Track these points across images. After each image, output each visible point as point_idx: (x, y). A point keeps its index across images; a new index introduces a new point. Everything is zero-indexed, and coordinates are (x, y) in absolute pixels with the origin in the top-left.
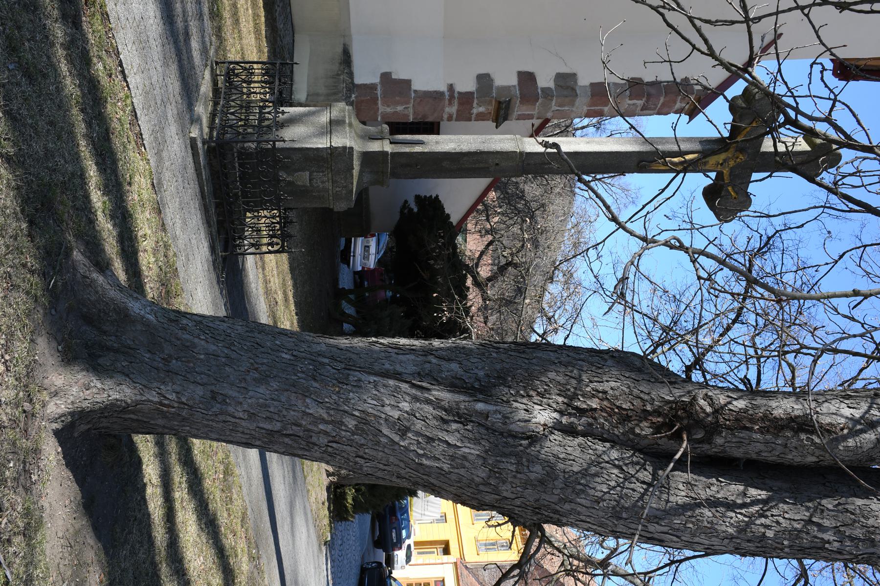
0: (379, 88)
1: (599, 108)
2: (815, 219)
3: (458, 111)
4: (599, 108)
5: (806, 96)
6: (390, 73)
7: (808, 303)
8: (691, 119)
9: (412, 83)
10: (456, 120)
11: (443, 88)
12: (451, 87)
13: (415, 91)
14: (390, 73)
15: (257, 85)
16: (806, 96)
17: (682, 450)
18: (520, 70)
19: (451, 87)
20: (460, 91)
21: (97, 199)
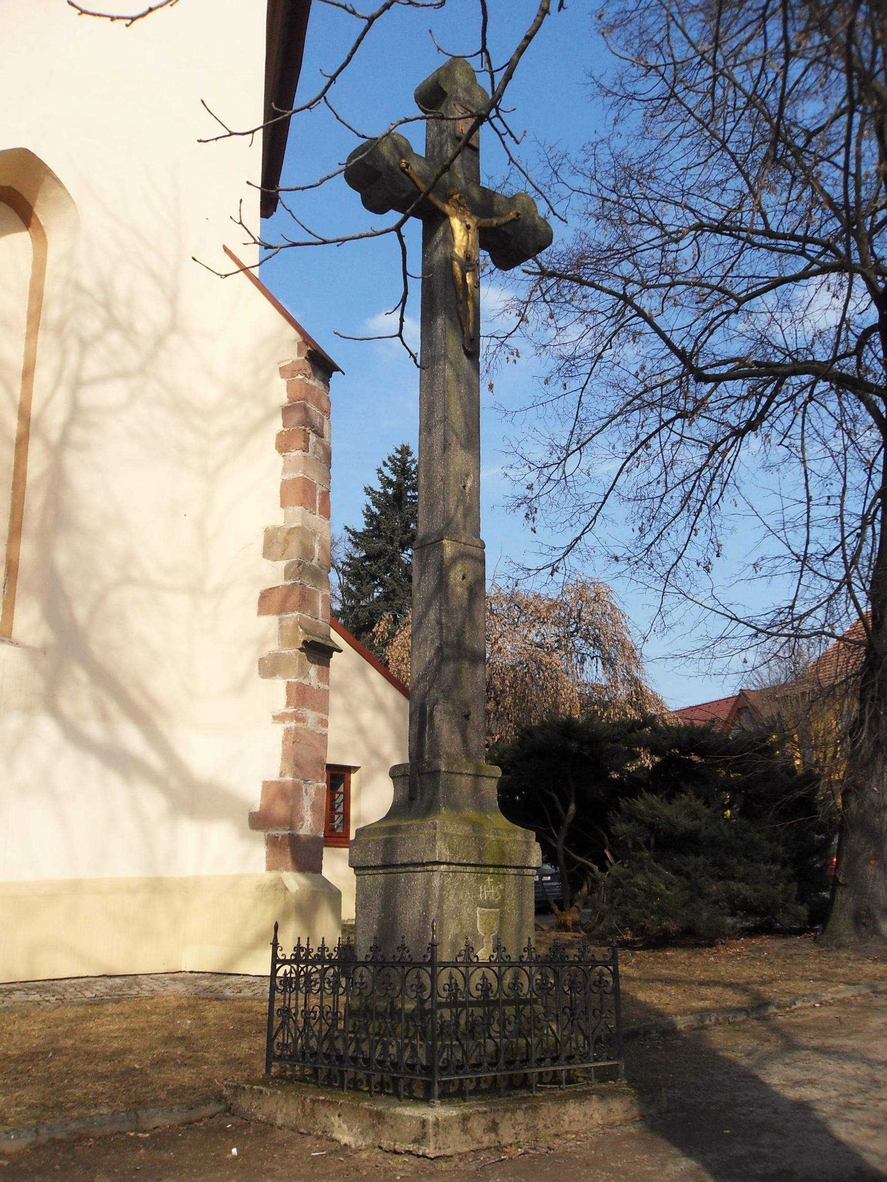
0: (275, 833)
1: (318, 497)
2: (231, 134)
3: (314, 709)
4: (318, 497)
5: (400, 237)
6: (251, 814)
7: (714, 281)
8: (338, 369)
9: (268, 779)
10: (327, 714)
11: (279, 730)
12: (279, 718)
13: (282, 774)
14: (251, 814)
15: (301, 1002)
16: (400, 237)
17: (318, 506)
18: (256, 612)
19: (279, 718)
20: (285, 703)
21: (878, 542)
